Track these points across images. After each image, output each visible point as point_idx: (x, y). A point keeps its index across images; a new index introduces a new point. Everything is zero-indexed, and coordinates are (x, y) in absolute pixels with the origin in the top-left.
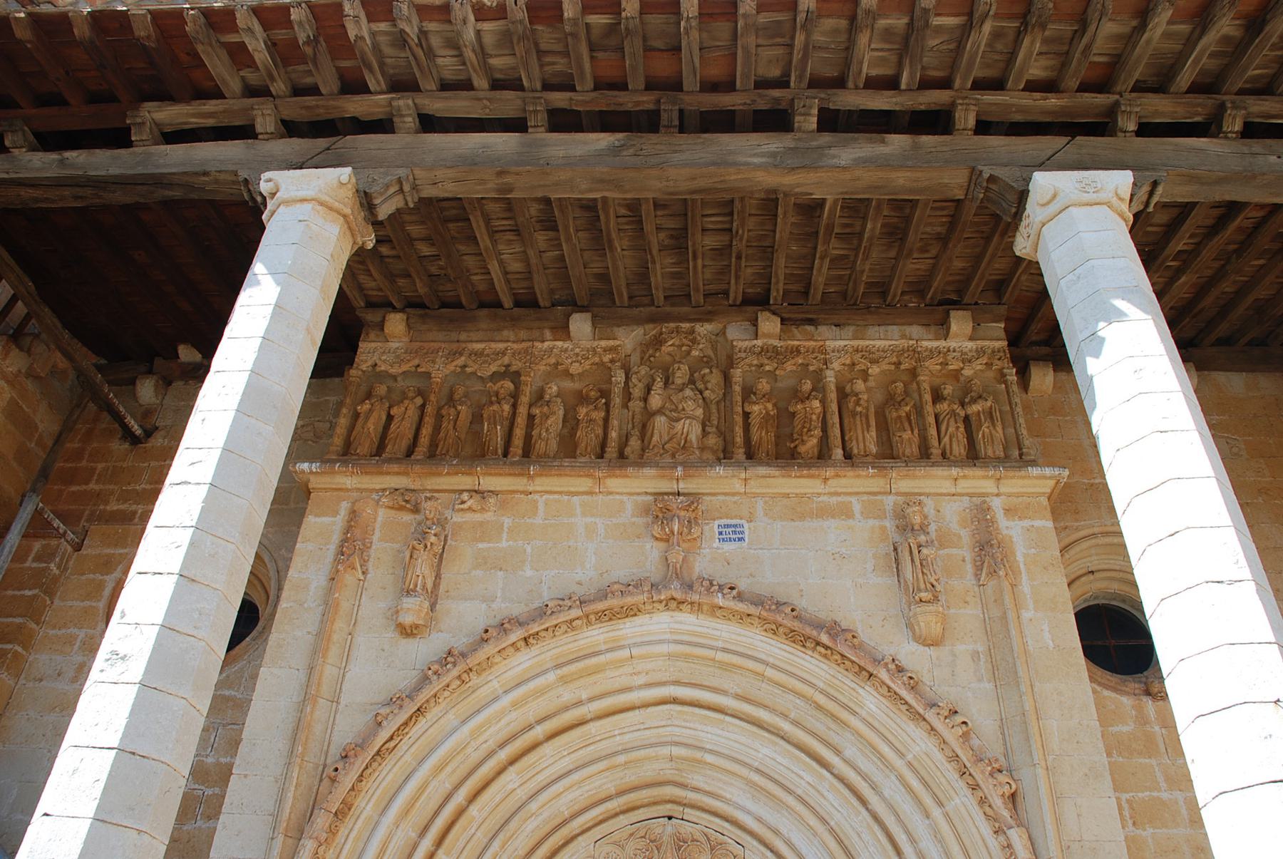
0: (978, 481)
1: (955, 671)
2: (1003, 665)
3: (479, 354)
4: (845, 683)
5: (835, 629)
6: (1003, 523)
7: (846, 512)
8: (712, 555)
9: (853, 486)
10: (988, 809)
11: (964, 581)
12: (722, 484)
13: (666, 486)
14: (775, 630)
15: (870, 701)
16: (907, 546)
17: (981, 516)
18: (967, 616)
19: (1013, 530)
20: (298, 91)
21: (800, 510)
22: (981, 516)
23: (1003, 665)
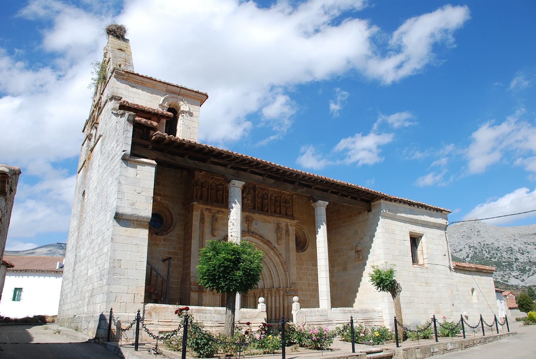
0: (288, 221)
1: (281, 249)
2: (287, 250)
3: (216, 179)
4: (269, 249)
5: (268, 241)
6: (289, 227)
7: (270, 222)
8: (254, 227)
9: (272, 219)
10: (96, 114)
11: (284, 236)
12: (256, 216)
13: (248, 215)
14: (262, 241)
15: (272, 252)
16: (278, 228)
17: (287, 225)
18: (284, 241)
19: (290, 228)
20: (268, 205)
21: (265, 221)
22: (287, 225)
23: (287, 250)
